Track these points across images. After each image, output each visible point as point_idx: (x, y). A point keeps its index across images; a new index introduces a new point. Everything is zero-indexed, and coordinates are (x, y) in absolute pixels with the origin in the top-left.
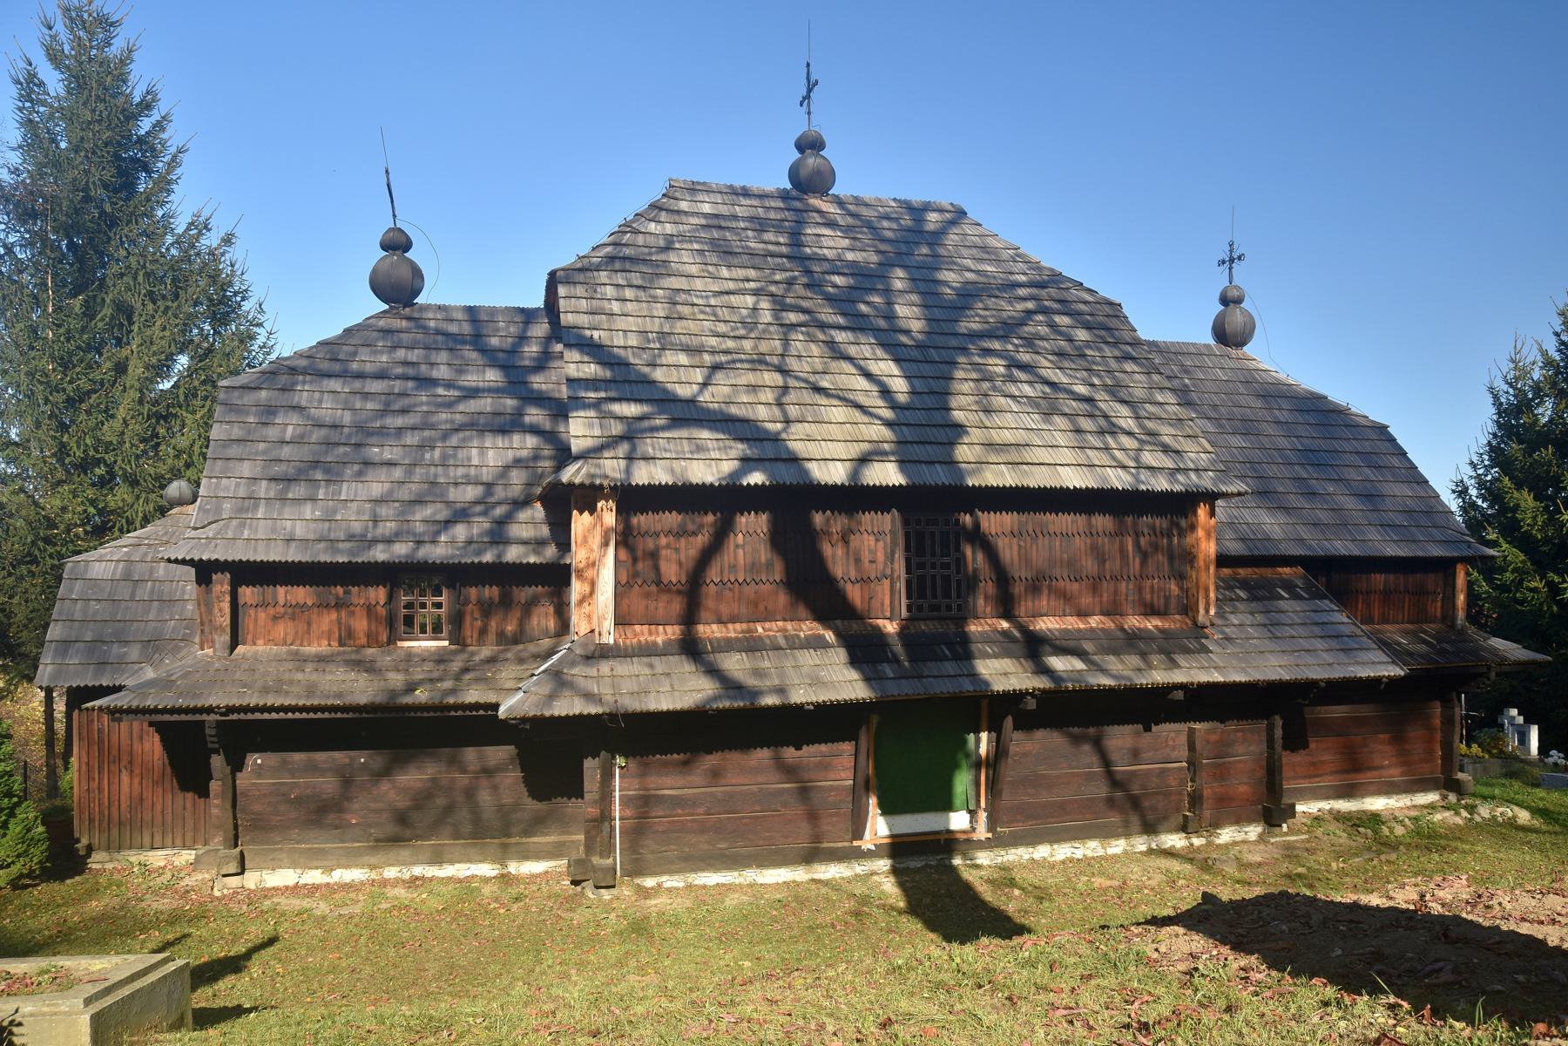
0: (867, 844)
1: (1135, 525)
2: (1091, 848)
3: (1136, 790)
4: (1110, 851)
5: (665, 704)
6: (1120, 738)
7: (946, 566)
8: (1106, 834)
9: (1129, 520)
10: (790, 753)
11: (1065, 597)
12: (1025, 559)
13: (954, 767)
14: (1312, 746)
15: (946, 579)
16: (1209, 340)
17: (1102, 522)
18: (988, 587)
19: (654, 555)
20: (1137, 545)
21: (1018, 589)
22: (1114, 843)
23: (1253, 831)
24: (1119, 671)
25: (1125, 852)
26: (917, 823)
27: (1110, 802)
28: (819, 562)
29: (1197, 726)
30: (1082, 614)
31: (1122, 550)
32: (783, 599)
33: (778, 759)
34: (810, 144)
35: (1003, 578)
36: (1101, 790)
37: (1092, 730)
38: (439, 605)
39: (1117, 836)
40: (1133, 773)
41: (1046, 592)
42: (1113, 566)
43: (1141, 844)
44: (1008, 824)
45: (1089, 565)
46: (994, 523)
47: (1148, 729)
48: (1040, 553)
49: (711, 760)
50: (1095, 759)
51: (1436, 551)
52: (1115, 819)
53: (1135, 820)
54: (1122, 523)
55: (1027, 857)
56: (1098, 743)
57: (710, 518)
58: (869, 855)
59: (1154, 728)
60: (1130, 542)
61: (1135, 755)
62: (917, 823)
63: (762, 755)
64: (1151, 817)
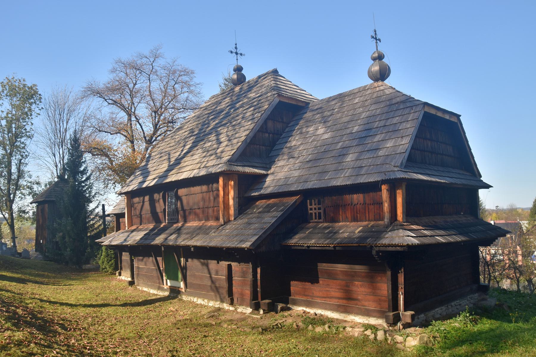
1: (212, 188)
8: (210, 299)
18: (181, 212)
26: (175, 284)
27: (212, 290)
29: (234, 264)
32: (151, 218)
34: (239, 70)
35: (184, 211)
36: (209, 283)
37: (206, 261)
39: (213, 300)
42: (207, 204)
46: (182, 192)
49: (145, 259)
50: (206, 271)
51: (372, 179)
53: (218, 296)
56: (207, 265)
62: (175, 284)
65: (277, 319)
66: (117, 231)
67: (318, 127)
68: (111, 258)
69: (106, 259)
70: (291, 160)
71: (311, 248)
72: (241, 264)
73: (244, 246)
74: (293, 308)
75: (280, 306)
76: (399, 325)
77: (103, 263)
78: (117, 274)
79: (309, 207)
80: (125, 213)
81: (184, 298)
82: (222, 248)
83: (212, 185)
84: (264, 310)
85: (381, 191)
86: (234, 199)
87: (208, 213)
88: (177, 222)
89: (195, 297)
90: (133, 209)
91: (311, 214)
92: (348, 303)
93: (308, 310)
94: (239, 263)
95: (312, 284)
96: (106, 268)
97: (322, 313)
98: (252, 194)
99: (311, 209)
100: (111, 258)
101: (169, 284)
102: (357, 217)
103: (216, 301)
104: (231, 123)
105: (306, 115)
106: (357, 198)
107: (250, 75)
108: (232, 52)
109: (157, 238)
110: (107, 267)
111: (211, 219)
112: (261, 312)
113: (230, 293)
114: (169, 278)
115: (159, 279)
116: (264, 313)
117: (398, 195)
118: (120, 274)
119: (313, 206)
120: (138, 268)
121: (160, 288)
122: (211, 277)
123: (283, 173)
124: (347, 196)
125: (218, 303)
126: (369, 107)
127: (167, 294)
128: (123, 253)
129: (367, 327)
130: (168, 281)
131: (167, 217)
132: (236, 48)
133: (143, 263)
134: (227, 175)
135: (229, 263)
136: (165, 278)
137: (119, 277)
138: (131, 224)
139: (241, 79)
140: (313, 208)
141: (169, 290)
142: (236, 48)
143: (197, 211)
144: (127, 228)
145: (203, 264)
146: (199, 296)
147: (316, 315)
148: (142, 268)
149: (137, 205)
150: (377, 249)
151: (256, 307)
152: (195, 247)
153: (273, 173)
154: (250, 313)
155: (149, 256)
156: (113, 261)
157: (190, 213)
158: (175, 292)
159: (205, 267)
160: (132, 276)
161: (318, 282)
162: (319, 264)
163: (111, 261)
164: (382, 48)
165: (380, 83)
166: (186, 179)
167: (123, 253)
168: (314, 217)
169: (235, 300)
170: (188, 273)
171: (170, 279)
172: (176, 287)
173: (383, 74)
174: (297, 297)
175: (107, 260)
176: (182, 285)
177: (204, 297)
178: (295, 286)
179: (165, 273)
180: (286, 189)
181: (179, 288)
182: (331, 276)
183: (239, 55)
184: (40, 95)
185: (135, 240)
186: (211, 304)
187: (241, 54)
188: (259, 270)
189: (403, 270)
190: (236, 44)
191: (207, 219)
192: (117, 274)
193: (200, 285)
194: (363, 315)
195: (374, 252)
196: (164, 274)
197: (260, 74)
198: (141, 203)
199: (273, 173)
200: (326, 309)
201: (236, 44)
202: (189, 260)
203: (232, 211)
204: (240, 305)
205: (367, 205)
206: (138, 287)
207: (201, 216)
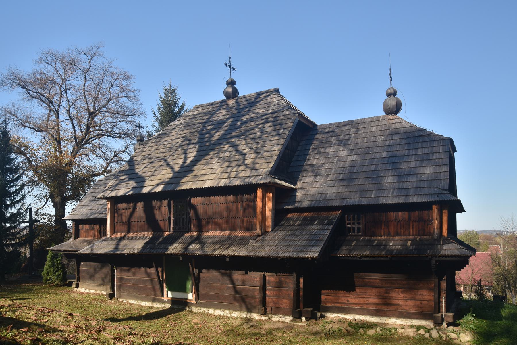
0: (165, 298)
1: (242, 198)
2: (227, 313)
3: (244, 295)
4: (233, 315)
5: (99, 252)
6: (238, 276)
7: (183, 215)
8: (233, 309)
9: (239, 197)
10: (148, 269)
11: (217, 224)
12: (205, 212)
13: (187, 279)
14: (358, 290)
15: (183, 219)
16: (382, 113)
17: (230, 198)
18: (195, 221)
19: (121, 215)
20: (242, 205)
21: (204, 222)
22: (234, 312)
23: (288, 319)
24: (233, 251)
25: (237, 317)
26: (179, 295)
27: (235, 299)
28: (154, 215)
29: (266, 274)
30: (222, 230)
31: (237, 208)
32: (146, 226)
33: (146, 271)
34: (231, 83)
35: (199, 219)
36: (232, 293)
37: (228, 272)
38: (349, 224)
39: (236, 310)
40: (242, 289)
41: (211, 223)
42: (233, 214)
43: (244, 315)
44: (203, 299)
45: (225, 214)
46: (195, 201)
47: (247, 273)
48: (210, 210)
49: (133, 270)
50: (228, 282)
51: (425, 199)
52: (237, 304)
53: (244, 307)
54: (237, 198)
55: (207, 312)
56: (230, 276)
57: (132, 204)
58: (165, 302)
59: (249, 273)
60: (240, 204)
61: (244, 283)
62: (179, 295)
63: (143, 269)
64: (249, 306)
65: (316, 326)
66: (75, 238)
67: (339, 148)
68: (58, 268)
69: (52, 269)
70: (318, 177)
71: (363, 259)
72: (278, 274)
73: (308, 255)
74: (326, 315)
75: (319, 314)
76: (445, 325)
77: (48, 273)
78: (74, 286)
79: (347, 221)
80: (106, 220)
81: (195, 309)
82: (277, 258)
83: (243, 195)
84: (306, 318)
85: (432, 209)
86: (272, 211)
87: (234, 223)
88: (189, 230)
89: (210, 308)
90: (116, 215)
91: (350, 228)
92: (385, 308)
93: (344, 316)
94: (276, 273)
95: (347, 292)
96: (51, 279)
97: (361, 318)
98: (286, 207)
99: (349, 224)
100: (58, 268)
101: (170, 295)
102: (400, 232)
103: (241, 311)
104: (247, 136)
105: (316, 137)
106: (401, 215)
107: (245, 90)
108: (226, 65)
109: (170, 247)
110: (54, 278)
111: (238, 229)
112: (304, 319)
113: (264, 302)
114: (170, 289)
115: (154, 290)
116: (307, 321)
117: (444, 214)
118: (77, 286)
119: (352, 221)
120: (121, 279)
121: (161, 301)
122: (234, 288)
123: (309, 188)
124: (392, 213)
125: (246, 313)
126: (62, 89)
127: (168, 306)
128: (82, 263)
129: (419, 328)
130: (169, 292)
131: (172, 226)
132: (230, 62)
133: (130, 274)
134: (266, 187)
135: (262, 274)
136: (165, 289)
137: (75, 289)
138: (114, 231)
139: (234, 94)
140: (349, 222)
141: (170, 302)
142: (230, 62)
143: (220, 221)
144: (109, 236)
145: (223, 274)
146: (216, 307)
147: (355, 320)
148: (127, 279)
149: (123, 211)
150: (437, 259)
151: (297, 316)
152: (232, 257)
153: (301, 188)
154: (292, 321)
155: (140, 266)
156: (60, 272)
157: (208, 223)
158: (179, 305)
159: (226, 278)
160: (113, 289)
161: (354, 290)
162: (355, 274)
163: (57, 271)
164: (396, 86)
165: (394, 116)
166: (213, 187)
167: (82, 263)
168: (352, 231)
169: (269, 309)
170: (201, 284)
171: (170, 290)
172: (182, 299)
173: (396, 109)
174: (329, 305)
175: (54, 270)
176: (190, 296)
177: (224, 308)
178: (326, 296)
179: (167, 284)
180: (322, 205)
181: (187, 299)
182: (367, 286)
183: (232, 69)
184: (140, 104)
185: (133, 249)
186: (235, 314)
187: (233, 69)
188: (301, 280)
189: (445, 277)
190: (230, 58)
191: (233, 229)
192: (74, 286)
193: (218, 296)
194: (404, 318)
195: (433, 262)
196: (165, 285)
197: (259, 90)
198: (131, 210)
199: (301, 188)
200: (363, 314)
201: (230, 58)
202: (204, 271)
203: (269, 222)
204: (275, 314)
205: (411, 222)
206: (121, 300)
207: (224, 226)
